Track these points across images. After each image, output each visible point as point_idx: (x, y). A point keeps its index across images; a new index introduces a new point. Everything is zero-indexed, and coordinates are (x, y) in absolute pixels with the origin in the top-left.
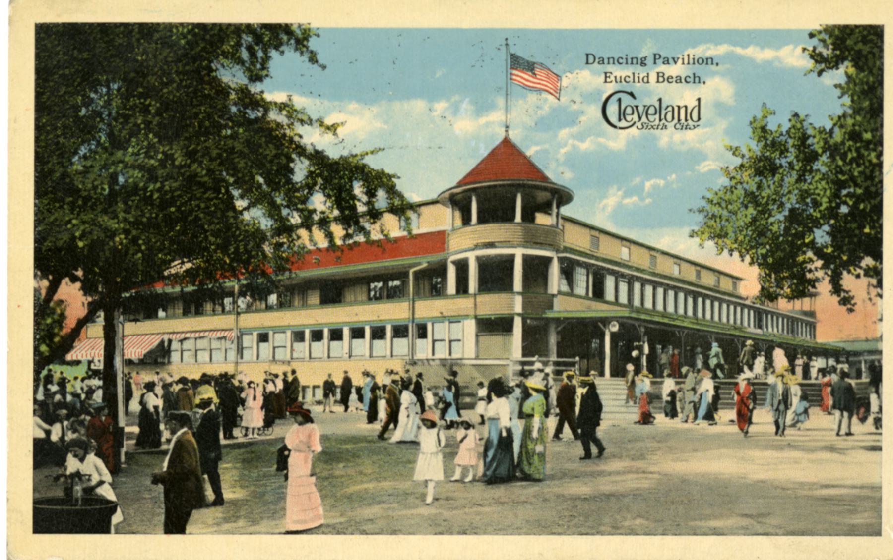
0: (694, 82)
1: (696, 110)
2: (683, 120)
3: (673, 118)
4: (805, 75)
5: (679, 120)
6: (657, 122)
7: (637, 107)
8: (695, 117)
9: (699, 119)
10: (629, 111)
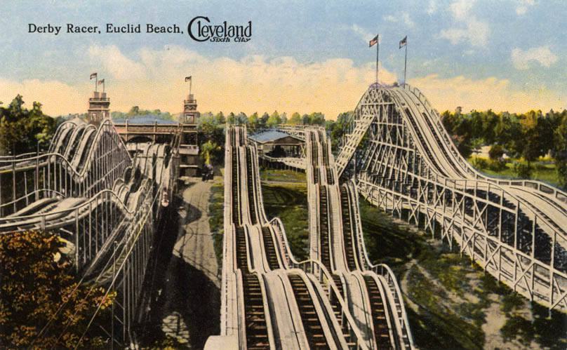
0: (175, 32)
1: (248, 28)
2: (240, 34)
3: (234, 34)
4: (242, 34)
5: (238, 35)
6: (223, 37)
7: (210, 27)
8: (248, 34)
9: (250, 35)
10: (205, 29)
